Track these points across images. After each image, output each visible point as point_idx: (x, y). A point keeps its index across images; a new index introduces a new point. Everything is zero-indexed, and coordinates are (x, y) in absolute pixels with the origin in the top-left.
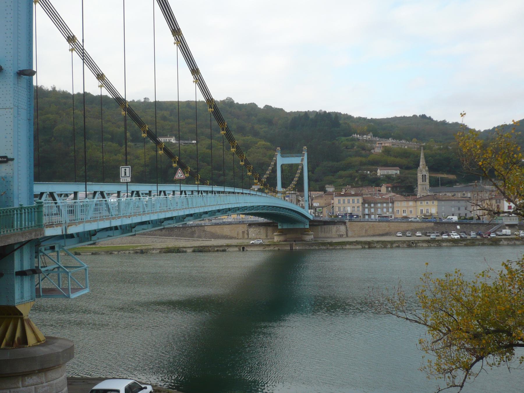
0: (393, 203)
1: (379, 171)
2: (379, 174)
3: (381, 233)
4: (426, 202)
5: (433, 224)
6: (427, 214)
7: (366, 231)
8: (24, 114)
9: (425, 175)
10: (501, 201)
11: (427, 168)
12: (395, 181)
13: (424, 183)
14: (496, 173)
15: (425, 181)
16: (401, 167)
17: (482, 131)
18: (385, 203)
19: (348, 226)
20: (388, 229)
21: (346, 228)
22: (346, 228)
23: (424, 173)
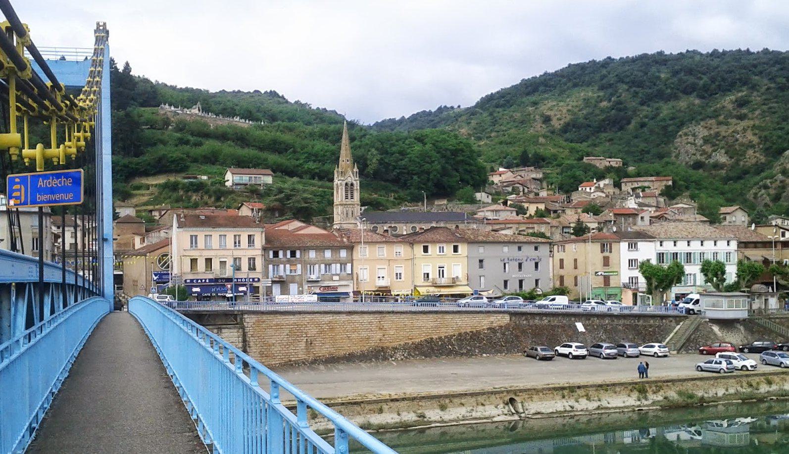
0: (350, 248)
1: (229, 176)
2: (228, 184)
3: (356, 349)
4: (438, 245)
5: (507, 318)
6: (444, 281)
7: (310, 344)
8: (377, 450)
9: (352, 185)
10: (614, 246)
11: (356, 170)
12: (273, 198)
13: (349, 201)
14: (626, 166)
15: (352, 197)
16: (278, 170)
17: (598, 61)
18: (328, 248)
19: (250, 331)
20: (379, 335)
21: (244, 335)
22: (244, 335)
23: (349, 180)
